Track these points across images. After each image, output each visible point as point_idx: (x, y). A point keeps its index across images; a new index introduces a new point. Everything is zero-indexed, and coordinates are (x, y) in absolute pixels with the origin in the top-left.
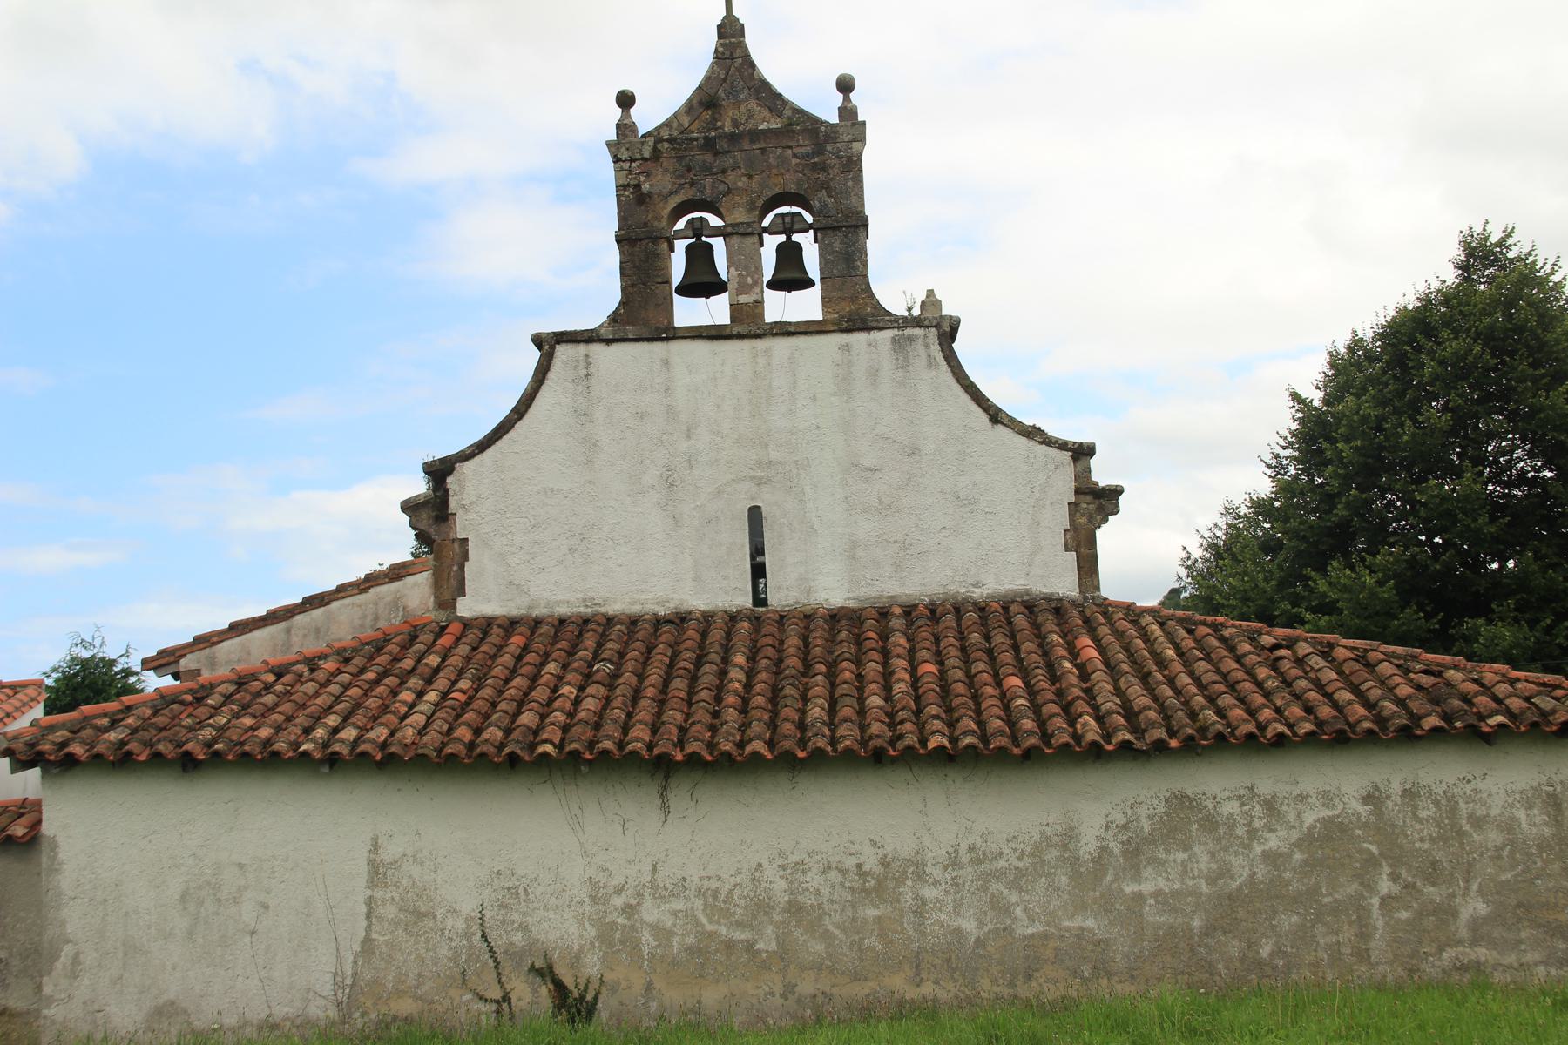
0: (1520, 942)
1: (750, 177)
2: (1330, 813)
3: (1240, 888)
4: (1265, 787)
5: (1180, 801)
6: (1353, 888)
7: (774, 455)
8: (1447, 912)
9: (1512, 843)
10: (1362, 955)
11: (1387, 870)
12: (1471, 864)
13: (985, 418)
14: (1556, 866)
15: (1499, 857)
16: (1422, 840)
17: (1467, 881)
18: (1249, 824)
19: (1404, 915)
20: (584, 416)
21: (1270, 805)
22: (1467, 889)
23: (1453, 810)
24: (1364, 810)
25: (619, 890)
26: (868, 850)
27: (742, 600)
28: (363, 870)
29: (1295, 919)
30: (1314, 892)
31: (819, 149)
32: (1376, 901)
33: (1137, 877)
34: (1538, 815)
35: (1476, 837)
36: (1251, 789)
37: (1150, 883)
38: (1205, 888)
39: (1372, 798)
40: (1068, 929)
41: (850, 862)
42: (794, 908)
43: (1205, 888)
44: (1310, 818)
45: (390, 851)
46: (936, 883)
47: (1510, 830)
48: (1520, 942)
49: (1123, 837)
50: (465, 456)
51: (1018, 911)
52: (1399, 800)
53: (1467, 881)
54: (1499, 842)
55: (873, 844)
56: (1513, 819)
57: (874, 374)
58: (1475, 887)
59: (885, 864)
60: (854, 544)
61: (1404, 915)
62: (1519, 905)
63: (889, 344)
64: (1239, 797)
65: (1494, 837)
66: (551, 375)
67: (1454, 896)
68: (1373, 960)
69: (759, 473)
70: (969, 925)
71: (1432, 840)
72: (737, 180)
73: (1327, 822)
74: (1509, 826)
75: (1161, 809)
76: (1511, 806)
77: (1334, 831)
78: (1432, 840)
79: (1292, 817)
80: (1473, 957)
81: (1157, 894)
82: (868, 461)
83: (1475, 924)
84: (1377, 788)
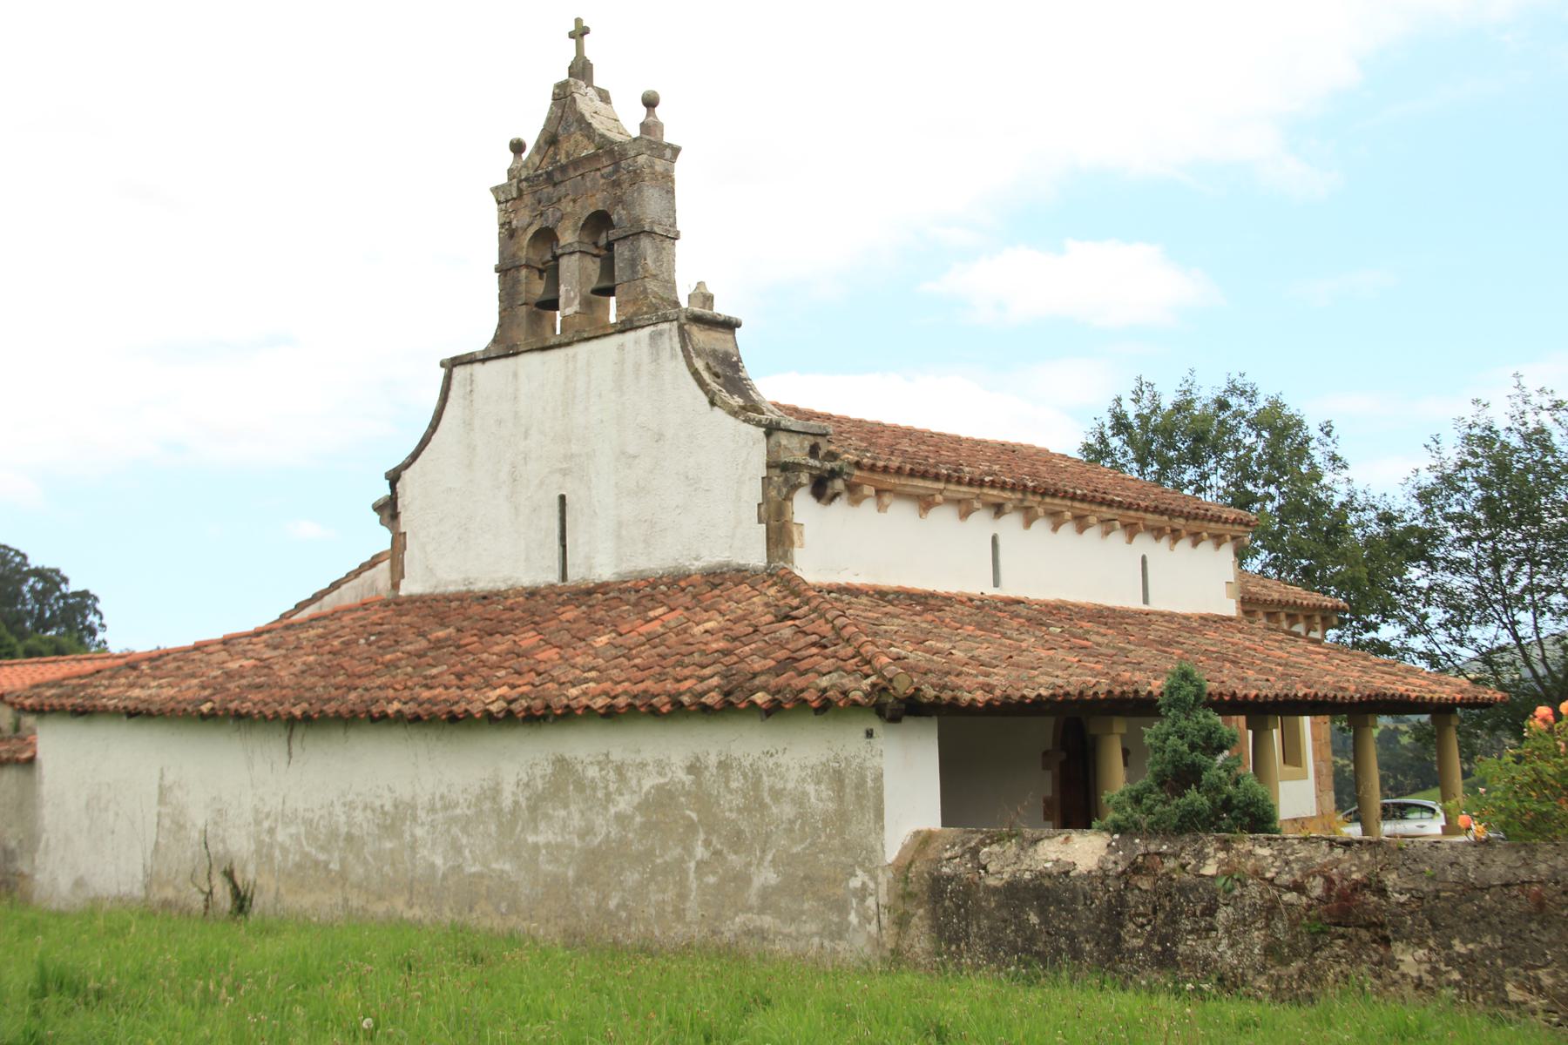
0: (802, 913)
1: (574, 201)
2: (662, 780)
3: (600, 845)
4: (617, 755)
5: (562, 763)
6: (677, 852)
7: (575, 448)
8: (743, 879)
9: (801, 816)
10: (679, 914)
11: (702, 836)
12: (768, 835)
13: (705, 400)
14: (836, 842)
15: (791, 830)
16: (731, 810)
17: (763, 851)
18: (606, 787)
19: (711, 879)
20: (468, 425)
21: (619, 770)
22: (762, 858)
23: (757, 784)
24: (688, 779)
25: (268, 816)
26: (386, 794)
27: (553, 577)
28: (155, 792)
29: (636, 876)
30: (649, 854)
31: (616, 164)
32: (692, 865)
33: (536, 830)
34: (826, 793)
35: (775, 810)
36: (607, 755)
37: (544, 836)
38: (577, 844)
39: (694, 769)
40: (494, 870)
41: (378, 803)
42: (350, 838)
43: (577, 844)
44: (647, 784)
45: (170, 778)
46: (423, 824)
47: (801, 805)
48: (802, 913)
49: (527, 794)
50: (406, 465)
51: (467, 852)
52: (715, 771)
53: (763, 851)
54: (791, 816)
55: (390, 789)
56: (805, 793)
57: (637, 367)
58: (770, 857)
59: (396, 807)
60: (620, 524)
61: (711, 879)
62: (806, 878)
63: (647, 339)
64: (599, 763)
65: (788, 811)
66: (452, 394)
67: (749, 864)
68: (688, 919)
69: (565, 465)
70: (439, 861)
71: (740, 811)
72: (567, 206)
73: (659, 788)
74: (800, 800)
75: (549, 771)
76: (804, 780)
77: (662, 800)
78: (740, 811)
79: (634, 782)
80: (758, 923)
81: (548, 845)
82: (631, 450)
83: (766, 894)
84: (698, 759)
